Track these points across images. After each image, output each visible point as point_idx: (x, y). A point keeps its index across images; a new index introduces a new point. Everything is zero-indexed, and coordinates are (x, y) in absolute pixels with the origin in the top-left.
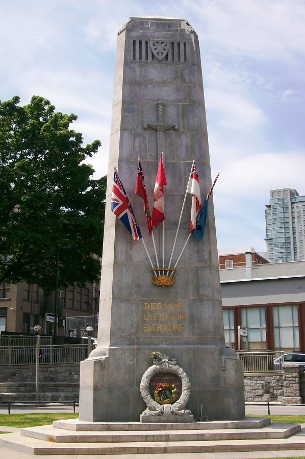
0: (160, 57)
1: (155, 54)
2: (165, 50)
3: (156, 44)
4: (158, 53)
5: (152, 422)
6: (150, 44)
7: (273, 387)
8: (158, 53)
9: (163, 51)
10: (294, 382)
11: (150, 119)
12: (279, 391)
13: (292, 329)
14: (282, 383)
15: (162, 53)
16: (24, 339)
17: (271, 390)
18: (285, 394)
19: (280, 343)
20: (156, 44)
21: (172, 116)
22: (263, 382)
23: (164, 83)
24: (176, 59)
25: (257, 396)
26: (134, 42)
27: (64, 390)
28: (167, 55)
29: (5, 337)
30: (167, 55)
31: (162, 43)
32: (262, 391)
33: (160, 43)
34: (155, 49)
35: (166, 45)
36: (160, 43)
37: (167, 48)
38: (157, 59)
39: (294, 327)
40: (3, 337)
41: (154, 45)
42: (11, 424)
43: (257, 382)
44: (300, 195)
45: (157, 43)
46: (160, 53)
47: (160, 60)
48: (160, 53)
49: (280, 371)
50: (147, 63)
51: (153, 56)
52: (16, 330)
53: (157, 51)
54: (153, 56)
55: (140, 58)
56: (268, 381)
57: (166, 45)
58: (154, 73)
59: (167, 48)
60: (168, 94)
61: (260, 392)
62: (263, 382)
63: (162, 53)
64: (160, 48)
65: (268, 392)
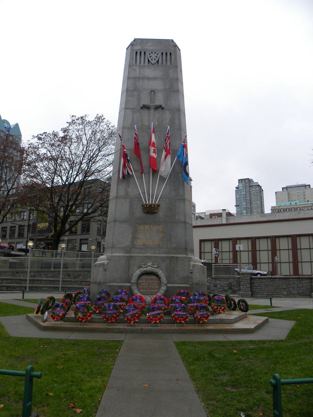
0: (153, 62)
1: (150, 60)
2: (156, 57)
3: (151, 54)
4: (152, 59)
6: (147, 53)
7: (234, 285)
8: (152, 59)
9: (156, 58)
10: (247, 282)
11: (146, 101)
13: (229, 258)
14: (240, 283)
15: (155, 59)
17: (233, 287)
18: (241, 290)
19: (249, 256)
20: (151, 54)
21: (160, 100)
22: (228, 282)
23: (155, 79)
24: (164, 62)
25: (224, 290)
26: (136, 53)
28: (158, 61)
30: (158, 61)
31: (155, 53)
32: (227, 288)
33: (153, 53)
34: (150, 57)
35: (158, 54)
36: (153, 53)
38: (151, 63)
39: (230, 259)
41: (149, 54)
42: (5, 288)
44: (255, 182)
45: (152, 53)
46: (153, 60)
48: (153, 60)
51: (149, 61)
54: (149, 61)
55: (140, 63)
57: (158, 54)
58: (149, 72)
59: (158, 56)
60: (158, 85)
61: (226, 288)
62: (228, 282)
63: (155, 59)
64: (154, 56)
65: (231, 289)
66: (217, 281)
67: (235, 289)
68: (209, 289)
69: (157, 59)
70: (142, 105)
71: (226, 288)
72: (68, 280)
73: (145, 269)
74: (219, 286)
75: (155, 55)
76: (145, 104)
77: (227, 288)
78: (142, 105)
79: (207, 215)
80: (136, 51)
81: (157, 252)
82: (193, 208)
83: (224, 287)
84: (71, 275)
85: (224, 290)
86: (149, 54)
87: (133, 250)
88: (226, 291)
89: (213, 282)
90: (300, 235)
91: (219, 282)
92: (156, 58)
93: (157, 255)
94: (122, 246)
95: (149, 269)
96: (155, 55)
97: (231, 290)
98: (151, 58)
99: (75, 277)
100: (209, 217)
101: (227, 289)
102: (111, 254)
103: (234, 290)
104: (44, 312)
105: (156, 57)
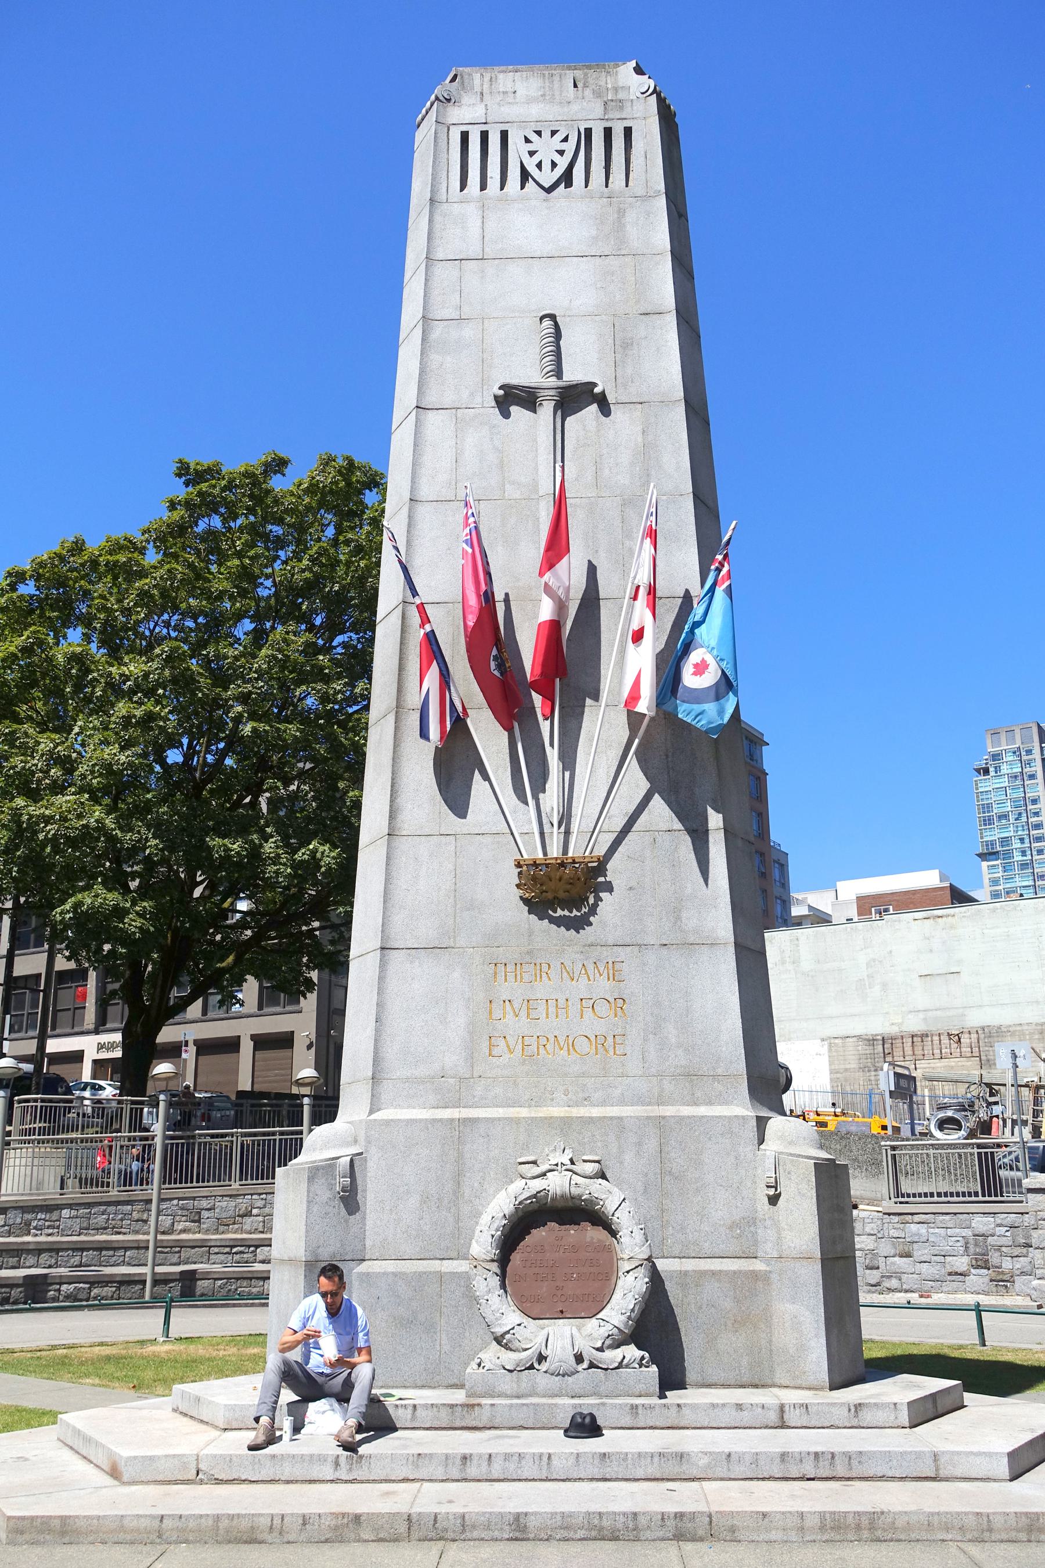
0: (547, 177)
2: (561, 153)
3: (534, 137)
4: (539, 166)
5: (499, 1396)
6: (517, 148)
8: (539, 166)
9: (557, 158)
12: (1021, 1263)
15: (554, 165)
16: (278, 1137)
17: (994, 1258)
22: (967, 1233)
25: (950, 1274)
26: (465, 137)
27: (28, 1224)
29: (264, 1134)
31: (554, 133)
33: (546, 134)
34: (532, 153)
36: (546, 134)
37: (570, 147)
40: (172, 1138)
41: (527, 140)
43: (950, 1232)
45: (539, 133)
46: (546, 166)
47: (547, 185)
48: (546, 166)
49: (227, 1183)
50: (506, 200)
51: (525, 175)
52: (309, 1067)
53: (536, 159)
56: (982, 1229)
61: (961, 1263)
62: (967, 1233)
63: (554, 165)
64: (547, 148)
66: (914, 1227)
67: (1007, 1264)
68: (871, 1268)
69: (563, 163)
70: (500, 388)
71: (961, 1263)
72: (190, 1236)
73: (537, 1185)
74: (920, 1252)
75: (556, 142)
76: (514, 381)
77: (965, 1260)
78: (500, 388)
79: (846, 903)
80: (464, 128)
81: (597, 1096)
82: (776, 873)
83: (948, 1259)
84: (205, 1214)
85: (950, 1274)
86: (527, 140)
87: (479, 1091)
88: (961, 1278)
89: (894, 1233)
90: (10, 1282)
91: (923, 1229)
92: (557, 158)
93: (595, 1112)
94: (422, 1071)
95: (557, 1184)
96: (556, 142)
97: (985, 1271)
98: (536, 159)
99: (222, 1224)
100: (853, 913)
101: (963, 1268)
102: (371, 1112)
103: (1003, 1273)
104: (347, 936)
105: (561, 153)
